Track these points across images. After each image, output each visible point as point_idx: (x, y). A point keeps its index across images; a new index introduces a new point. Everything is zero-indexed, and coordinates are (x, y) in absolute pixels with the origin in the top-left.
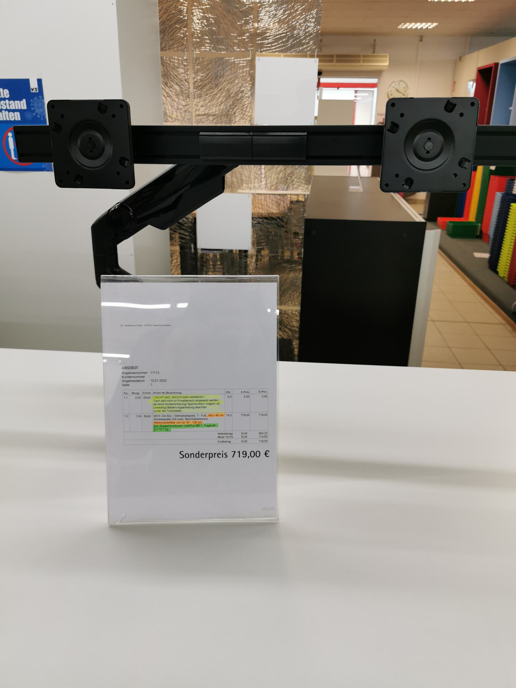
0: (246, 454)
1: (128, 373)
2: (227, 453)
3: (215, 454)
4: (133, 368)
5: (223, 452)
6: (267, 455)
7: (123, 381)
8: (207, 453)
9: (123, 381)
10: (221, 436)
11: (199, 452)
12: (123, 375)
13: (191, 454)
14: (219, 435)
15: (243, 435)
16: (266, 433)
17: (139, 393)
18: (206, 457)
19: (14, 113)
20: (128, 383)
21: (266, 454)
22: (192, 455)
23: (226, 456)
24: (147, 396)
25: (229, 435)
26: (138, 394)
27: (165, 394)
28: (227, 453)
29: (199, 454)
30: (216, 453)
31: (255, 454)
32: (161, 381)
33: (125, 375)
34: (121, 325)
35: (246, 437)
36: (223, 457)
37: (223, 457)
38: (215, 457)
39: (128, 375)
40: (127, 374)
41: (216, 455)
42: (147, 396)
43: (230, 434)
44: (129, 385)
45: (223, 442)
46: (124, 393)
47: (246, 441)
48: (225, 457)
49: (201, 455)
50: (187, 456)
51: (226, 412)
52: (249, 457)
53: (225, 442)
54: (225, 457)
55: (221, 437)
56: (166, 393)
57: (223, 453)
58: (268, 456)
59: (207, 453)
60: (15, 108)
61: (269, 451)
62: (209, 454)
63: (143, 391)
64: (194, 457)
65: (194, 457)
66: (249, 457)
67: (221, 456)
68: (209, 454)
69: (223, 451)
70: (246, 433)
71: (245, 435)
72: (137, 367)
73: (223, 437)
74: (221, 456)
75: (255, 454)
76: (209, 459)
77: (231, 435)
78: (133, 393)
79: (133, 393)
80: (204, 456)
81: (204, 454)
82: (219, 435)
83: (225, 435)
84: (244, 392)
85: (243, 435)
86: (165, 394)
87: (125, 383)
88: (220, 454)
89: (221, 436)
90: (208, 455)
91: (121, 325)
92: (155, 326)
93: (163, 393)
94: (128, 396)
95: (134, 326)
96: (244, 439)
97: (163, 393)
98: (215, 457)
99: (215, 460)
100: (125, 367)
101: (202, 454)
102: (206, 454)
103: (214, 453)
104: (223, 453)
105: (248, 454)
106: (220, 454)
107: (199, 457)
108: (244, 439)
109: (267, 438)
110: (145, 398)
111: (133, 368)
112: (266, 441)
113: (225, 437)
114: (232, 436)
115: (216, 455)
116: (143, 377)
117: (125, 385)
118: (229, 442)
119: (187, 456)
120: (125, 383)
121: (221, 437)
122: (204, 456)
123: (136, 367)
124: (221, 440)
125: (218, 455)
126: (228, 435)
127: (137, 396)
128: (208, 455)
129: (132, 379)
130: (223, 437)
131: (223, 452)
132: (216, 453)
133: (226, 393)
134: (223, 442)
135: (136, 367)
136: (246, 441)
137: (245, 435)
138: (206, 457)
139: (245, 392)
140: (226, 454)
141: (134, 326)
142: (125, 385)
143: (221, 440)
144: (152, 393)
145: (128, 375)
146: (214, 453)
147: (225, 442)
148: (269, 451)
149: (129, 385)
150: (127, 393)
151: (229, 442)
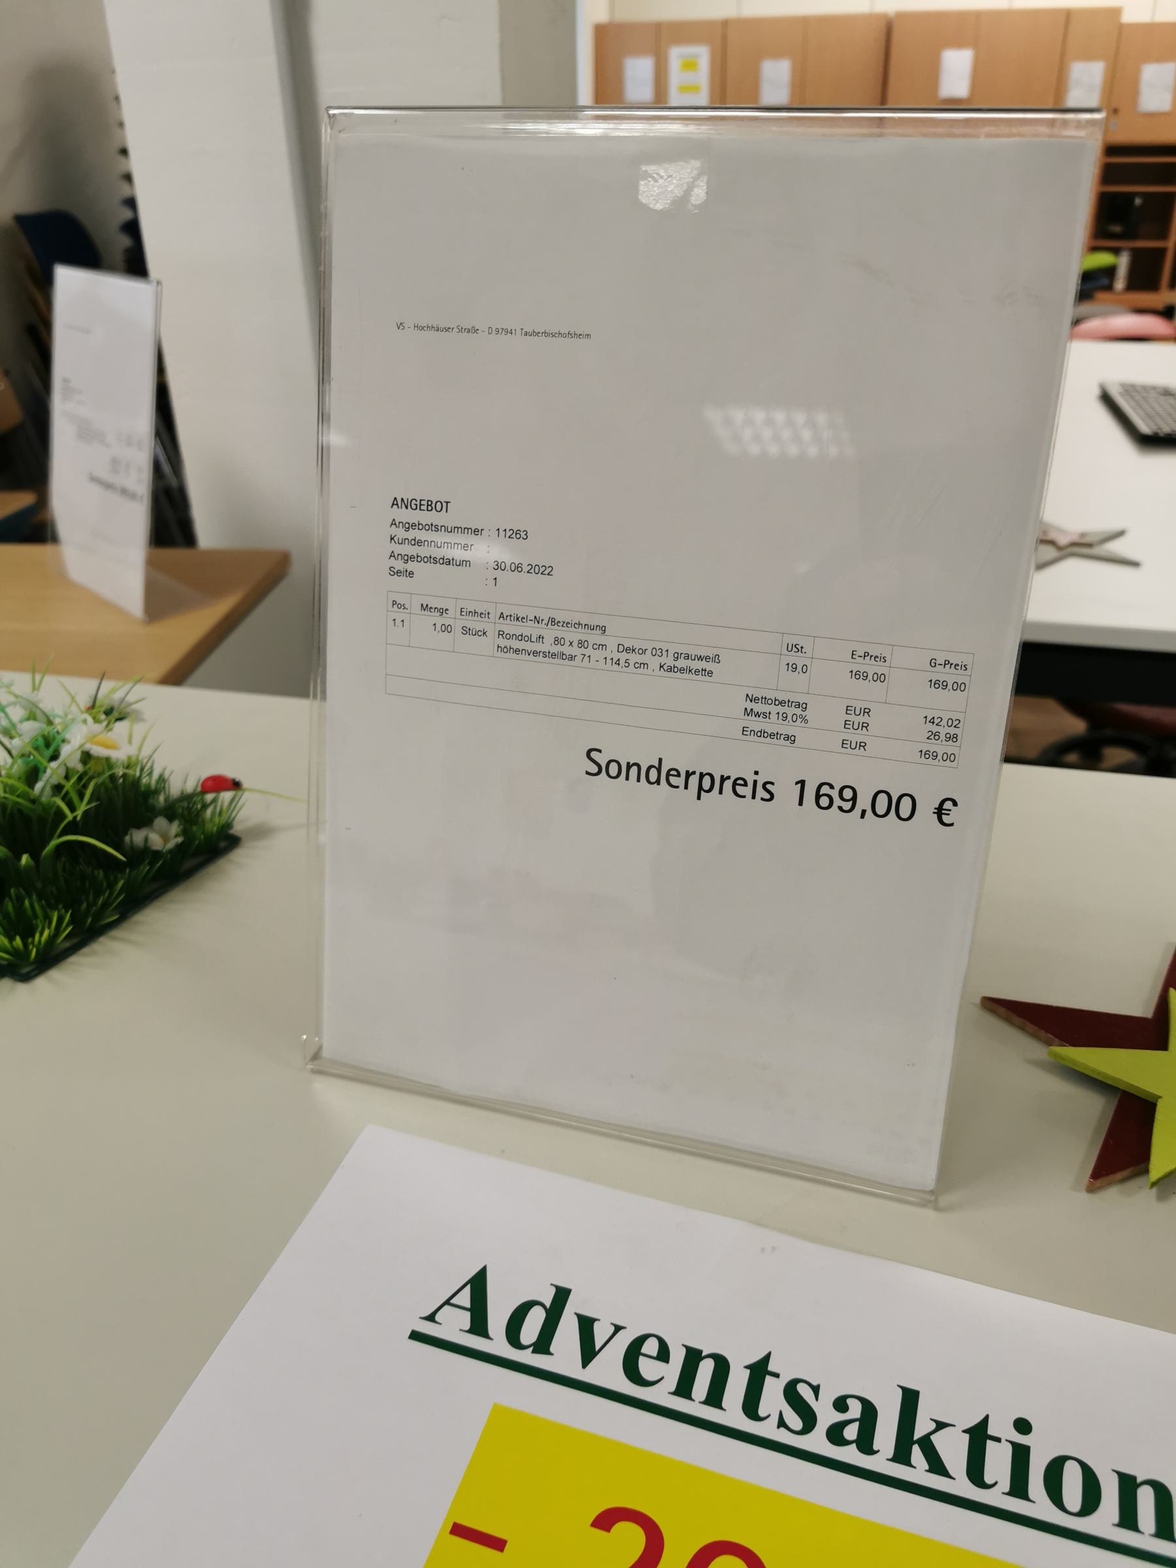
0: (854, 799)
1: (413, 526)
2: (772, 784)
3: (723, 779)
4: (430, 506)
5: (756, 777)
6: (945, 819)
7: (392, 555)
8: (694, 773)
9: (392, 555)
10: (759, 707)
11: (660, 760)
12: (394, 531)
13: (629, 766)
14: (749, 705)
15: (852, 718)
16: (954, 723)
17: (447, 610)
18: (686, 787)
19: (145, 845)
20: (411, 566)
21: (940, 812)
22: (634, 770)
23: (767, 796)
24: (475, 624)
25: (790, 711)
26: (442, 611)
27: (543, 625)
28: (772, 784)
29: (659, 770)
30: (728, 778)
31: (894, 806)
32: (534, 569)
33: (400, 533)
34: (400, 326)
35: (865, 726)
36: (754, 797)
37: (754, 797)
38: (721, 792)
39: (411, 534)
40: (407, 530)
41: (728, 785)
42: (475, 624)
43: (798, 705)
44: (411, 574)
45: (762, 733)
46: (394, 603)
47: (862, 745)
48: (763, 799)
49: (668, 775)
50: (613, 769)
51: (779, 656)
52: (864, 812)
53: (772, 735)
54: (763, 799)
55: (758, 715)
56: (545, 621)
57: (755, 782)
58: (952, 825)
59: (694, 773)
60: (140, 749)
61: (955, 804)
62: (702, 776)
63: (461, 604)
64: (638, 780)
65: (638, 780)
66: (864, 812)
67: (746, 791)
68: (702, 776)
69: (756, 773)
70: (867, 711)
71: (862, 719)
72: (447, 503)
73: (766, 715)
74: (746, 791)
75: (894, 806)
76: (699, 798)
77: (799, 711)
78: (424, 608)
79: (424, 608)
80: (679, 781)
81: (679, 775)
82: (749, 705)
83: (774, 709)
84: (866, 654)
85: (852, 718)
86: (543, 625)
87: (399, 565)
88: (746, 784)
89: (759, 707)
90: (694, 780)
91: (400, 326)
92: (526, 334)
93: (537, 620)
94: (405, 617)
95: (447, 329)
96: (856, 737)
97: (537, 620)
98: (721, 792)
99: (721, 802)
100: (402, 500)
101: (672, 772)
102: (688, 774)
103: (722, 776)
104: (755, 782)
105: (864, 802)
106: (746, 784)
107: (658, 782)
108: (856, 737)
109: (957, 744)
110: (466, 631)
111: (430, 506)
112: (950, 758)
113: (774, 716)
114: (804, 714)
115: (728, 785)
116: (465, 547)
117: (398, 573)
118: (788, 738)
119: (613, 769)
120: (399, 565)
121: (758, 715)
122: (679, 781)
123: (444, 504)
124: (756, 724)
125: (735, 784)
126: (785, 709)
127: (440, 621)
128: (694, 780)
129: (423, 551)
130: (766, 715)
131: (756, 777)
132: (728, 778)
133: (784, 651)
134: (762, 733)
135: (444, 504)
136: (862, 745)
137: (862, 719)
138: (686, 787)
139: (868, 658)
140: (768, 786)
141: (447, 329)
142: (398, 573)
143: (756, 724)
144: (494, 616)
145: (411, 534)
146: (722, 776)
147: (772, 735)
148: (955, 804)
149: (411, 574)
150: (402, 606)
151: (788, 738)
